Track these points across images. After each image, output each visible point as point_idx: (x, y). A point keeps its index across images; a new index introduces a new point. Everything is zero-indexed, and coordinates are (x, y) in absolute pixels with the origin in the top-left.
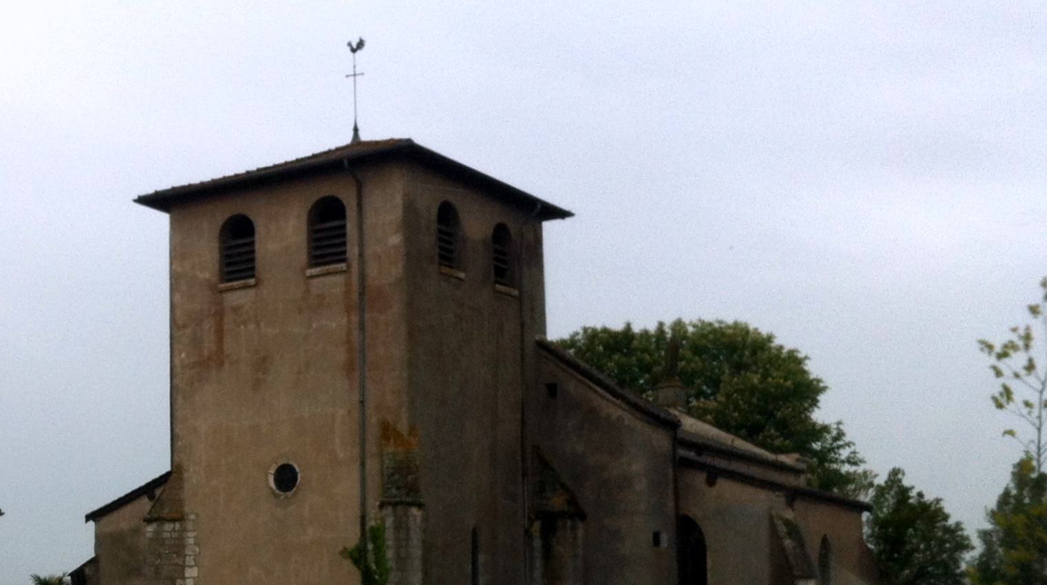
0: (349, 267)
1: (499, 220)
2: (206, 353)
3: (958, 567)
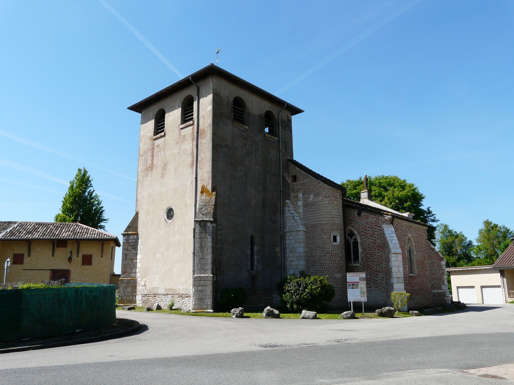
0: (193, 123)
2: (148, 165)
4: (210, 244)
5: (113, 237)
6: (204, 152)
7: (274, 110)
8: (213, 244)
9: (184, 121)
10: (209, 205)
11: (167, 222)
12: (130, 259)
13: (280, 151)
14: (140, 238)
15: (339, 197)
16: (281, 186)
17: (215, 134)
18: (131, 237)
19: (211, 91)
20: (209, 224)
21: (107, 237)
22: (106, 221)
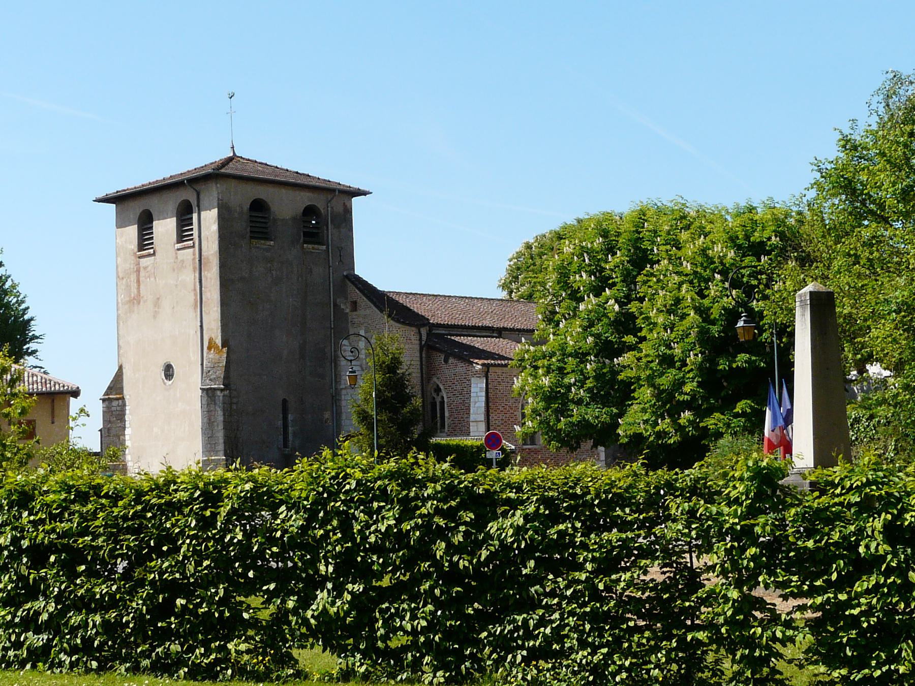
1: (138, 211)
2: (132, 296)
3: (303, 524)
4: (221, 418)
5: (72, 388)
6: (210, 291)
7: (319, 202)
8: (224, 418)
9: (181, 238)
10: (218, 366)
11: (165, 384)
12: (114, 436)
13: (329, 267)
14: (127, 404)
15: (413, 338)
16: (332, 319)
17: (223, 266)
18: (115, 403)
19: (216, 204)
20: (218, 393)
21: (62, 389)
22: (39, 340)
